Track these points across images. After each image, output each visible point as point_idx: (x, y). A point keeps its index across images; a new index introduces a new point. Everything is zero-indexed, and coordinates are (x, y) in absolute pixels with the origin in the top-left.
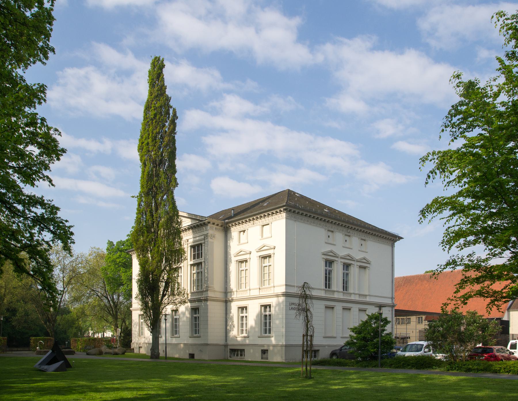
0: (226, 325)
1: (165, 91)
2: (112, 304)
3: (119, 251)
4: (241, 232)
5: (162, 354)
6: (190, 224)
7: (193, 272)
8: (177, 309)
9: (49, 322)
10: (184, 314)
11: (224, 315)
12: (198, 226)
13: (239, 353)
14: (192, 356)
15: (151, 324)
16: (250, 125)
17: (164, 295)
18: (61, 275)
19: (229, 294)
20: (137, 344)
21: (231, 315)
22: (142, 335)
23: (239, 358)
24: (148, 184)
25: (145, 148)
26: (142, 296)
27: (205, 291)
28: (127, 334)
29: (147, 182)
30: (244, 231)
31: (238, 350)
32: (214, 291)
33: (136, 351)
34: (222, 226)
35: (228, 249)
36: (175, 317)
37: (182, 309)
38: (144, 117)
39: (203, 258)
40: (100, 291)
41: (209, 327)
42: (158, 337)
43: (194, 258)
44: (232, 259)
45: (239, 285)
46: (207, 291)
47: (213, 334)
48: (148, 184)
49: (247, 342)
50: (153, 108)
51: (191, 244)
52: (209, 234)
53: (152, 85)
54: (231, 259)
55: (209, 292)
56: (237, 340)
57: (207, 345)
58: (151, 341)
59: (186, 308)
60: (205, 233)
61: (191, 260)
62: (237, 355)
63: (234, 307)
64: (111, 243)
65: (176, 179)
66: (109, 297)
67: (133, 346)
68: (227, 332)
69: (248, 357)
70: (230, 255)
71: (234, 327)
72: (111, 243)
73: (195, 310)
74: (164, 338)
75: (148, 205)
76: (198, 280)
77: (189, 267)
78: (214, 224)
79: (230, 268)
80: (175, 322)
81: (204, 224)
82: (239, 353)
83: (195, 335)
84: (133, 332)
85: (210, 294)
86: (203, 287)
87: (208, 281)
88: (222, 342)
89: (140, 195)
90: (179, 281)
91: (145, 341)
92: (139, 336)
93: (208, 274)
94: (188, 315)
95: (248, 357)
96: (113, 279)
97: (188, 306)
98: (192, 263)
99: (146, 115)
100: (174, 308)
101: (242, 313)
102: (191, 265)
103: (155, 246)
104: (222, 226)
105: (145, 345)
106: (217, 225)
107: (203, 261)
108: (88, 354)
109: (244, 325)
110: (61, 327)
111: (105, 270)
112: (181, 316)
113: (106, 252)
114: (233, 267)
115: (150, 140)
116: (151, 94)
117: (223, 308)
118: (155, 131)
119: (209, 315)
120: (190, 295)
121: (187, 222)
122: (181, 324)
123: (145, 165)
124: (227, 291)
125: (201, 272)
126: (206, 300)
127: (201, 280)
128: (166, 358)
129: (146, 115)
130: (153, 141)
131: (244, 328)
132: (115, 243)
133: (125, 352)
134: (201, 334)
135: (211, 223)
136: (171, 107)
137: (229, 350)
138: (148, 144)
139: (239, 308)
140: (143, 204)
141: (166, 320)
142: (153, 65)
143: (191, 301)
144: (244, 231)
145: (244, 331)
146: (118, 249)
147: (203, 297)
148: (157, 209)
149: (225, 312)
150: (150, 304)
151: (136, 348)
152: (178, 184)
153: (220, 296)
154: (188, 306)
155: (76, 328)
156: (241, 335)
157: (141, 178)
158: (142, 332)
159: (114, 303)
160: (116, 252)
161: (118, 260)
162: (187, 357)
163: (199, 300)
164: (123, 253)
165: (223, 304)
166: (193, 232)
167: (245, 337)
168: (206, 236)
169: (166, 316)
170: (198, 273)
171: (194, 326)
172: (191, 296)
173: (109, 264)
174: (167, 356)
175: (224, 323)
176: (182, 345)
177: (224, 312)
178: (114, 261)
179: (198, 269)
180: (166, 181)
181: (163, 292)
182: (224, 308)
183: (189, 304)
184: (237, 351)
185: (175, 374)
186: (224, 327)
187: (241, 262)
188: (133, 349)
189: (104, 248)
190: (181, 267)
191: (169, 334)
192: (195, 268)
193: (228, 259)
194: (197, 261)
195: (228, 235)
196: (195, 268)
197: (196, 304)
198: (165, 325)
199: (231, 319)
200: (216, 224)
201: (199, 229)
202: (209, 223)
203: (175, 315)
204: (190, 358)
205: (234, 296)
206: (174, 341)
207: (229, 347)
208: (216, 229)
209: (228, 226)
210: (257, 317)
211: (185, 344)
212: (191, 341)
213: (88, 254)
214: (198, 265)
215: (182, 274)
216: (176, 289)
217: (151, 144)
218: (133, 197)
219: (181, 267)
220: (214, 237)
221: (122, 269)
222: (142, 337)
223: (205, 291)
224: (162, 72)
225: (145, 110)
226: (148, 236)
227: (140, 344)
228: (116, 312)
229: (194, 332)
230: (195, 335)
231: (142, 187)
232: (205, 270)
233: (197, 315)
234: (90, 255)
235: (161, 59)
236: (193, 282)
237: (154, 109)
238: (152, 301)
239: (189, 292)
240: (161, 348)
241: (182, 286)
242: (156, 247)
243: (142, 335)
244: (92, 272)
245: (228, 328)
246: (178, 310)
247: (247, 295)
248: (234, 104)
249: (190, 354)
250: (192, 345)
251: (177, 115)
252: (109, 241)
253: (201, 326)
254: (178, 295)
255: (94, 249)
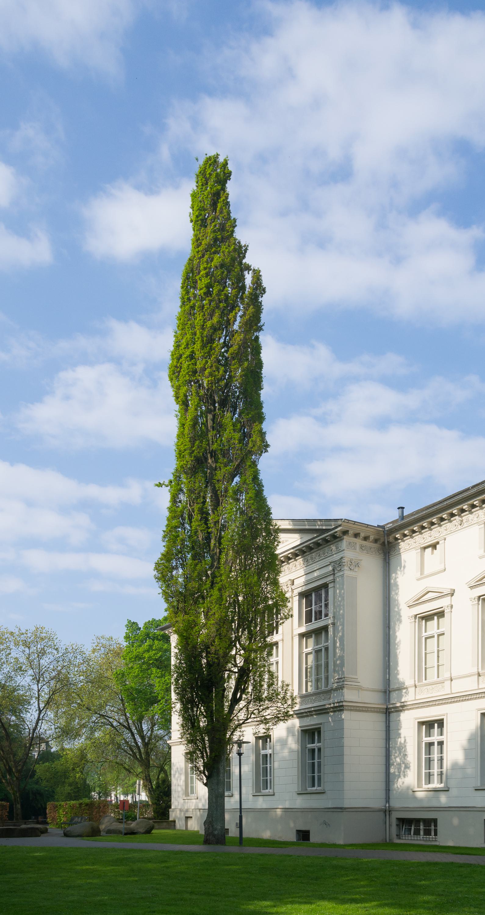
0: (388, 764)
1: (233, 232)
2: (139, 740)
3: (150, 638)
4: (425, 548)
5: (233, 832)
6: (298, 543)
7: (305, 650)
8: (269, 734)
9: (10, 774)
10: (283, 742)
11: (382, 743)
12: (318, 544)
13: (422, 827)
14: (304, 835)
15: (204, 767)
16: (396, 435)
17: (235, 701)
18: (35, 687)
19: (394, 695)
20: (181, 810)
21: (402, 740)
22: (192, 792)
23: (421, 839)
24: (193, 446)
25: (185, 366)
26: (182, 702)
27: (336, 689)
28: (162, 793)
29: (193, 441)
30: (434, 546)
31: (417, 821)
32: (359, 689)
33: (180, 825)
34: (376, 541)
35: (393, 593)
36: (263, 752)
37: (279, 731)
38: (183, 298)
39: (331, 615)
40: (117, 718)
41: (346, 769)
42: (223, 796)
43: (309, 620)
44: (402, 613)
45: (422, 670)
46: (341, 688)
47: (357, 784)
48: (193, 446)
49: (443, 799)
50: (203, 272)
51: (300, 590)
52: (345, 560)
53: (200, 222)
54: (399, 613)
55: (345, 691)
56: (415, 798)
57: (342, 809)
58: (207, 807)
59: (290, 730)
60: (336, 557)
61: (300, 625)
62: (417, 832)
63: (408, 725)
64: (133, 626)
65: (262, 434)
66: (133, 729)
67: (172, 816)
68: (388, 780)
69: (446, 837)
70: (398, 605)
71: (407, 767)
72: (133, 626)
73: (310, 734)
74: (237, 796)
75: (196, 496)
76: (318, 667)
77: (296, 639)
78: (356, 535)
79: (398, 634)
80: (263, 765)
81: (334, 537)
82: (422, 827)
83: (310, 789)
84: (173, 788)
85: (349, 695)
86: (331, 680)
87: (342, 665)
88: (379, 804)
89: (177, 478)
90: (273, 668)
91: (197, 804)
92: (187, 794)
93: (342, 649)
94: (293, 744)
95: (446, 837)
96: (139, 692)
97: (294, 726)
98: (303, 630)
99: (188, 293)
100: (261, 730)
101: (429, 734)
102: (302, 636)
103: (212, 587)
104: (376, 541)
105: (198, 813)
106: (366, 538)
107: (330, 621)
108: (66, 835)
109: (436, 764)
110: (44, 783)
111: (123, 675)
112: (278, 748)
113: (125, 644)
114: (405, 633)
115: (198, 345)
116: (197, 241)
117: (382, 726)
118: (209, 324)
119: (347, 742)
120: (298, 700)
121: (291, 541)
122: (276, 765)
123: (185, 404)
124: (389, 688)
125: (327, 649)
126: (339, 708)
127: (325, 669)
128: (241, 840)
129: (188, 293)
130: (203, 346)
131: (435, 770)
132: (141, 625)
133: (152, 828)
134: (326, 785)
135: (351, 532)
136: (248, 268)
137: (394, 822)
138: (192, 357)
139: (421, 723)
140: (182, 497)
141: (240, 754)
142: (203, 177)
143: (300, 715)
144: (434, 546)
145: (436, 778)
146: (148, 635)
147: (334, 699)
148: (217, 503)
149: (384, 736)
150: (203, 723)
151: (179, 819)
152: (267, 446)
153: (373, 699)
154: (294, 726)
155: (70, 785)
156: (425, 787)
157: (178, 436)
158: (192, 788)
159: (143, 737)
160: (142, 642)
161: (146, 655)
162: (292, 837)
163: (322, 711)
164: (156, 642)
165: (381, 718)
166: (306, 561)
167: (436, 791)
168: (338, 565)
169: (240, 746)
170: (317, 652)
171: (308, 769)
172: (301, 704)
173: (130, 666)
174: (244, 836)
175: (382, 760)
176: (279, 812)
177: (383, 735)
178: (138, 657)
179: (317, 642)
180: (237, 435)
181: (235, 694)
182: (382, 726)
183: (295, 722)
184: (419, 823)
185: (264, 898)
186: (383, 768)
187: (427, 618)
188: (174, 821)
189: (119, 636)
190: (276, 644)
191: (248, 789)
192: (311, 641)
193: (392, 614)
194: (316, 625)
195: (393, 561)
196: (311, 641)
197: (312, 721)
198: (241, 768)
199: (400, 749)
200: (362, 535)
201: (321, 552)
202: (345, 533)
203: (264, 748)
204: (298, 839)
205: (409, 698)
206: (261, 803)
207: (395, 815)
208: (361, 547)
209: (391, 539)
210: (470, 740)
211: (286, 810)
212: (300, 802)
213: (91, 649)
214: (319, 633)
215: (280, 659)
216: (265, 686)
217: (198, 354)
218: (160, 485)
219: (276, 644)
220: (357, 565)
221: (154, 670)
222: (190, 797)
223: (336, 689)
224: (223, 189)
225: (183, 284)
226: (196, 565)
227: (187, 811)
228: (148, 754)
229: (308, 782)
230: (310, 789)
231: (180, 455)
232: (335, 643)
233: (315, 745)
234: (94, 651)
235: (221, 160)
236: (305, 673)
237: (207, 275)
238: (209, 715)
239: (296, 693)
240: (230, 821)
241: (280, 679)
242: (217, 587)
243: (192, 792)
244: (98, 681)
245: (392, 770)
246: (269, 736)
247: (444, 691)
248: (368, 399)
249: (298, 832)
250: (303, 811)
251: (264, 284)
252: (129, 622)
253: (327, 769)
254: (270, 699)
255: (102, 641)
